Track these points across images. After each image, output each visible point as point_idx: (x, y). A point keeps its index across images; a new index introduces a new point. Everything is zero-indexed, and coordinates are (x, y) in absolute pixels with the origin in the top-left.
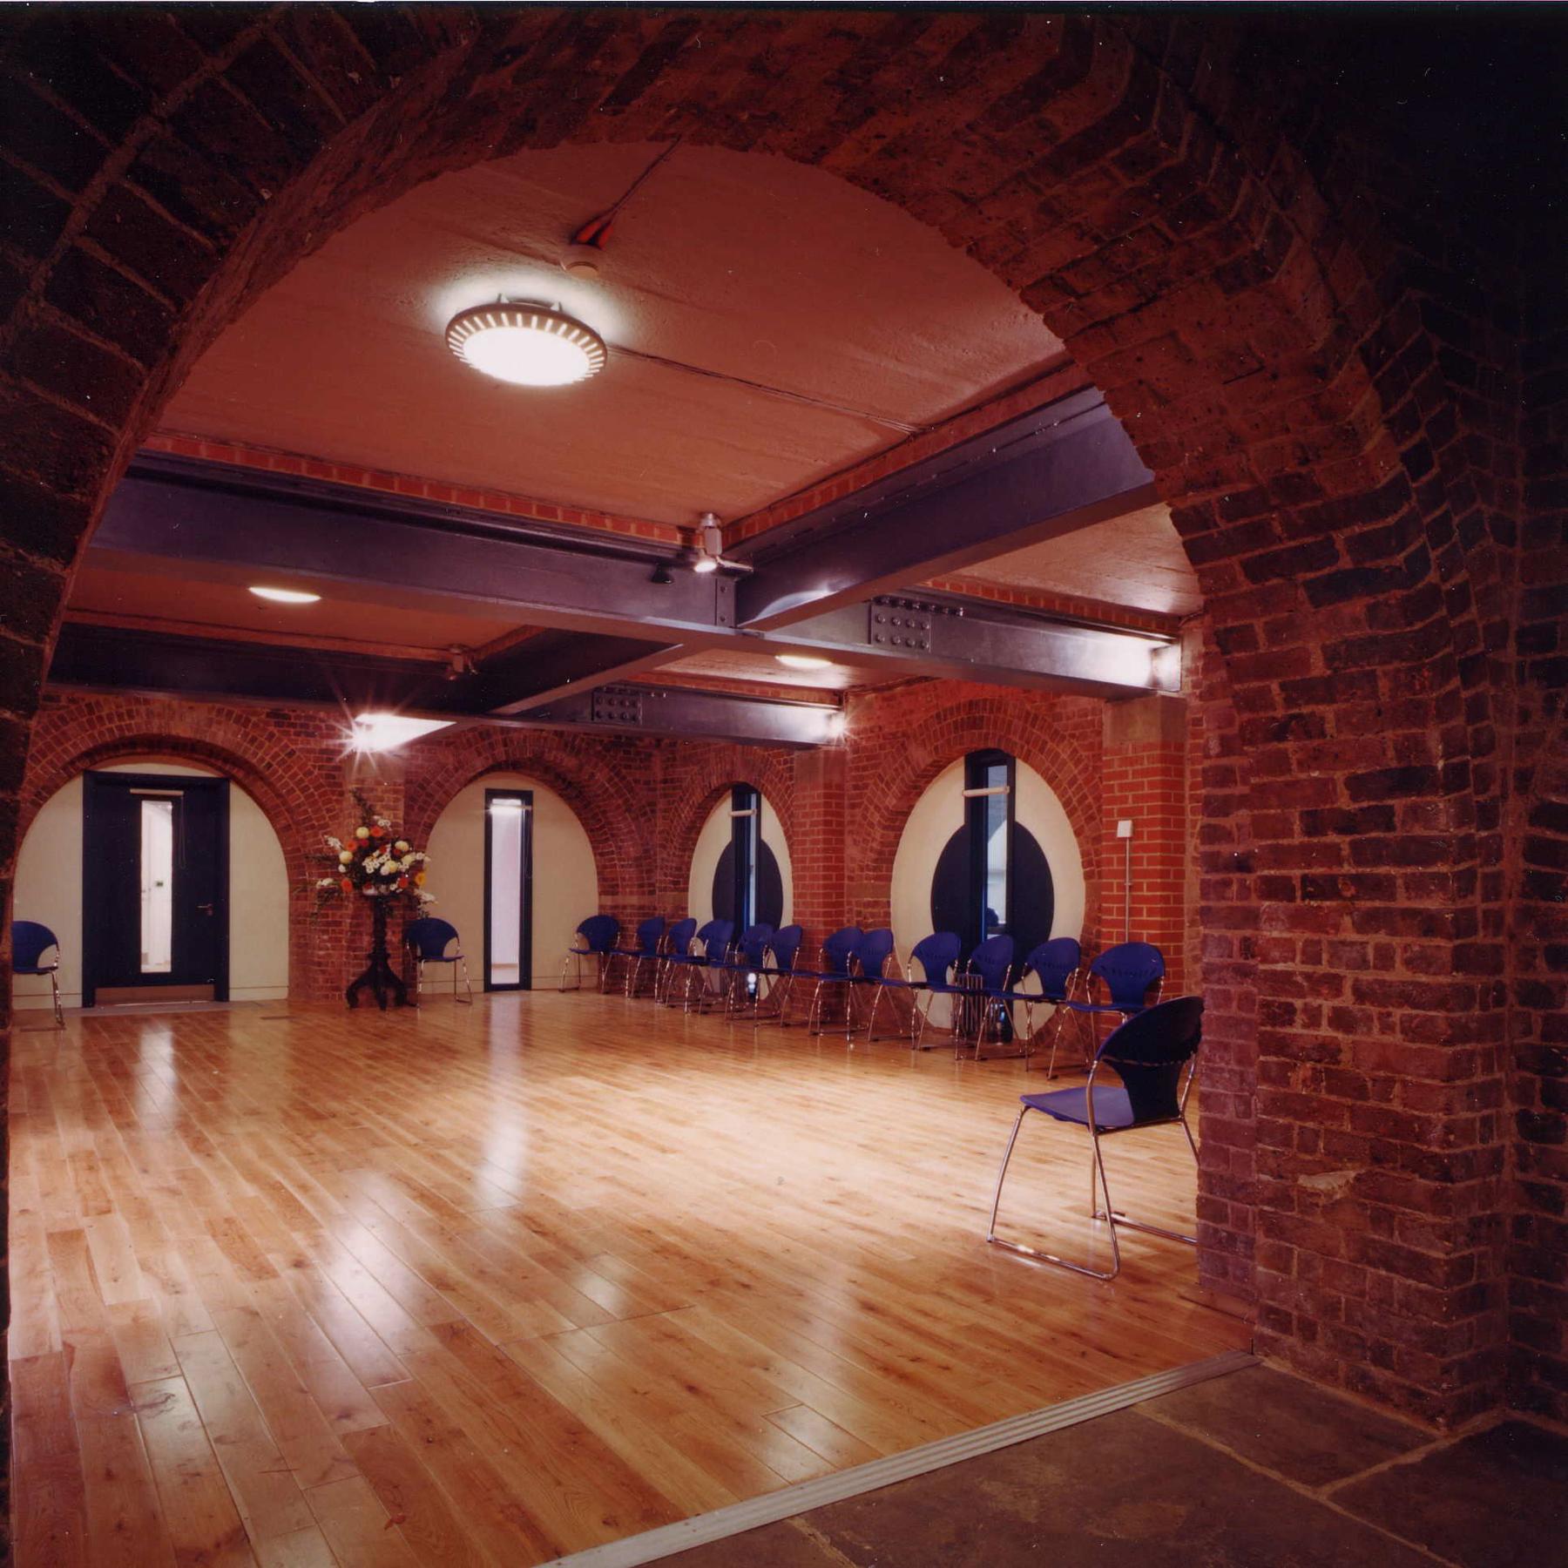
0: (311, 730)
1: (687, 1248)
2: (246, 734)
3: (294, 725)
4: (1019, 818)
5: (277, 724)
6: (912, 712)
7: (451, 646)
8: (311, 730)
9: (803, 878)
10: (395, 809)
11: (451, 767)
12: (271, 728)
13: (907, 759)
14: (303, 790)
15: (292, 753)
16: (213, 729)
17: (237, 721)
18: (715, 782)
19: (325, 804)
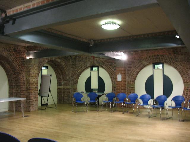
0: (20, 53)
1: (2, 119)
2: (9, 54)
3: (17, 52)
4: (99, 75)
5: (15, 52)
6: (143, 56)
7: (91, 39)
8: (20, 53)
9: (10, 92)
10: (37, 70)
11: (42, 62)
12: (14, 53)
13: (142, 63)
14: (19, 66)
15: (17, 58)
16: (3, 52)
17: (8, 51)
18: (88, 65)
19: (22, 69)
